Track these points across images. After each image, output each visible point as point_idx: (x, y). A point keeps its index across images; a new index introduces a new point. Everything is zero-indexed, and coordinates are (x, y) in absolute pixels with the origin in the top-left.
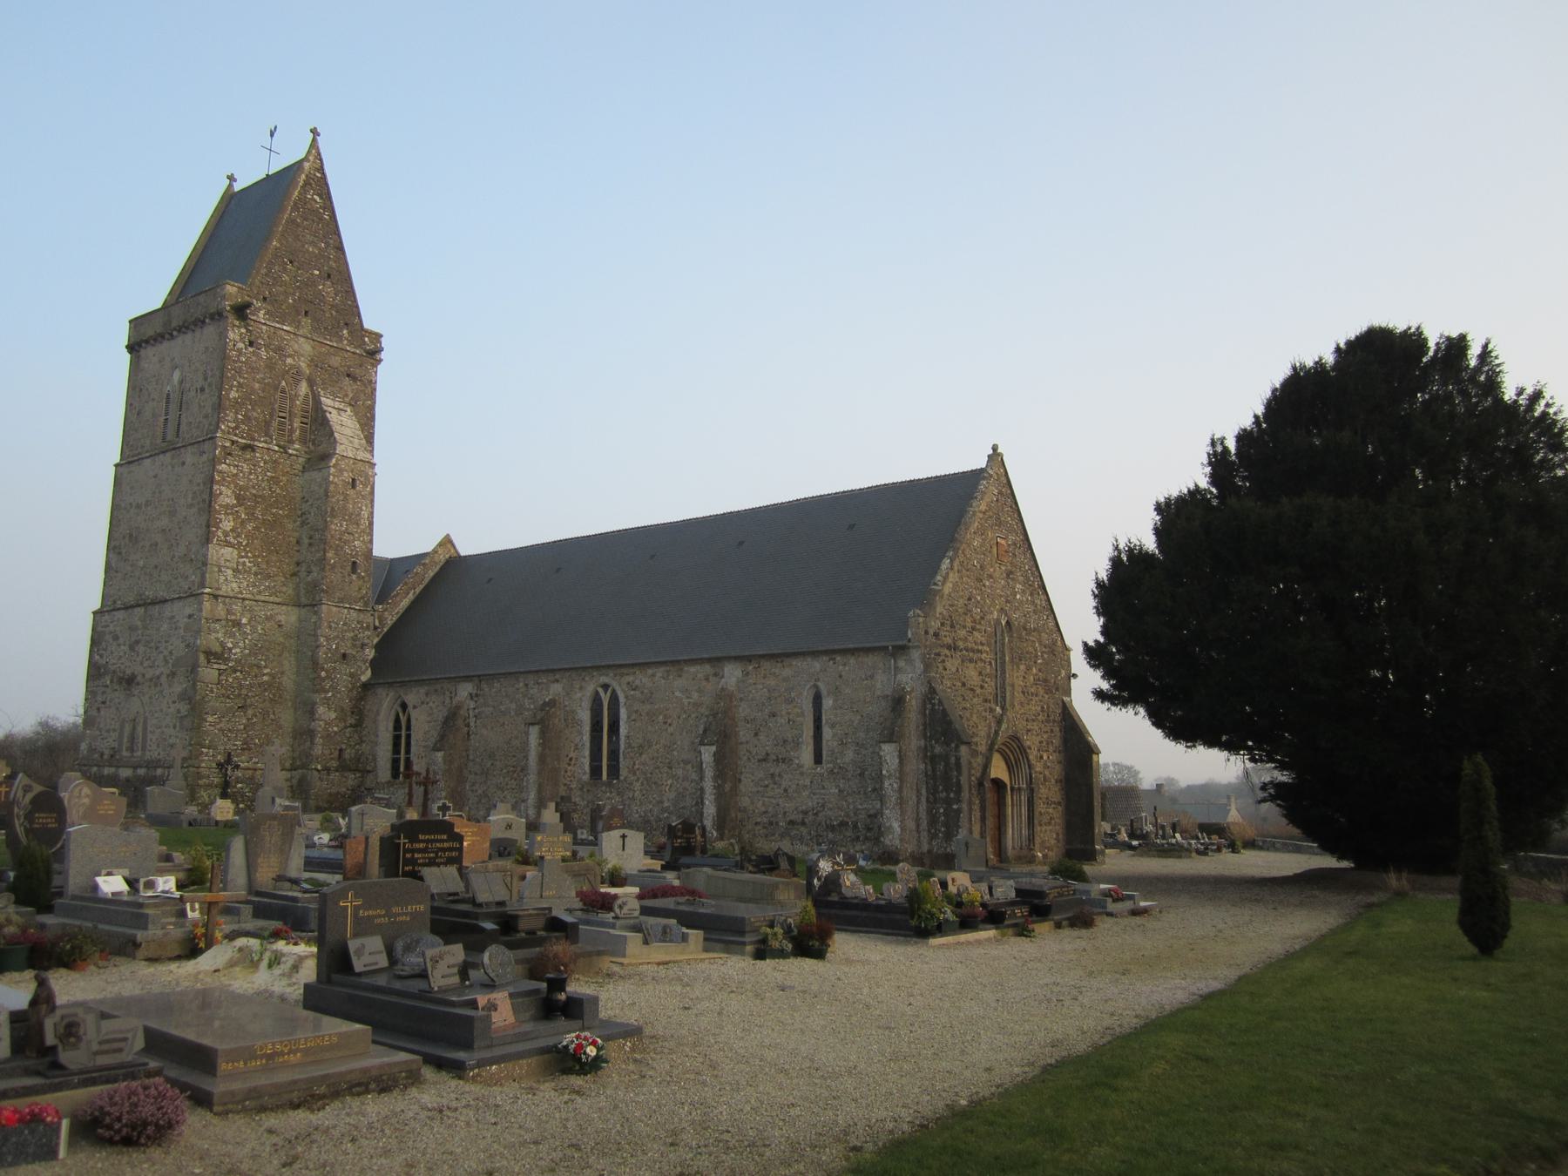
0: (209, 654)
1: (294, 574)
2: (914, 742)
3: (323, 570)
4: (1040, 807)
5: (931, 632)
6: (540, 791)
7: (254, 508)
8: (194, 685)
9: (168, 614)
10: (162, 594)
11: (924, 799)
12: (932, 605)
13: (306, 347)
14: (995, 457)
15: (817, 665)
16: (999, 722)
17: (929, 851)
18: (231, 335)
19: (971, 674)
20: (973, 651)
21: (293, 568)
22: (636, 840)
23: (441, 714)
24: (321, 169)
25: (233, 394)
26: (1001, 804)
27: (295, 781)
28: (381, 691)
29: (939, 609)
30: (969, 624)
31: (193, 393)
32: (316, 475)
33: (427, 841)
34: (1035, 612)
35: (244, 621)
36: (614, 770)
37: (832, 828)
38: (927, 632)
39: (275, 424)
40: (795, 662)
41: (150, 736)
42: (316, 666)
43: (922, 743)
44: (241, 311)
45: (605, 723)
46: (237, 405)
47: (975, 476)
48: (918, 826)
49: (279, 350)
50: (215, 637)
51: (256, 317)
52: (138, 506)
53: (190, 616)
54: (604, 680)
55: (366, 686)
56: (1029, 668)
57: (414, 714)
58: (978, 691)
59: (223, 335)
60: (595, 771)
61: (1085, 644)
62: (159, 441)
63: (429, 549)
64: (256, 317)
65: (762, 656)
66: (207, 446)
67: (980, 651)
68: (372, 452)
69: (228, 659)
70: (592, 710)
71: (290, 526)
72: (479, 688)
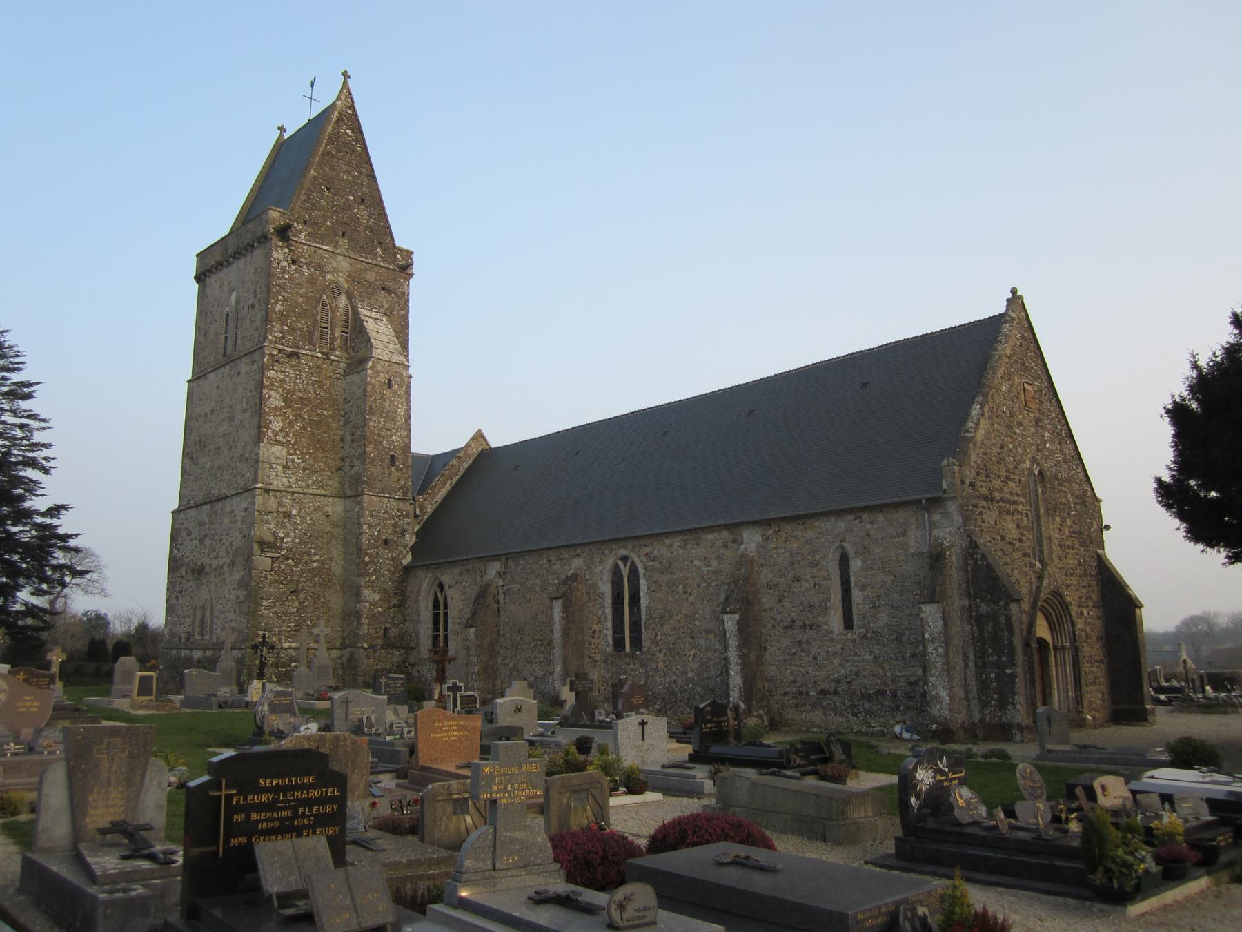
0: (262, 543)
1: (339, 469)
2: (957, 602)
3: (364, 463)
4: (1085, 667)
5: (967, 481)
6: (565, 665)
7: (301, 409)
8: (250, 572)
9: (228, 509)
10: (225, 492)
11: (971, 664)
12: (966, 453)
13: (344, 264)
14: (1015, 300)
15: (841, 525)
16: (1040, 577)
17: (982, 721)
18: (275, 254)
19: (1009, 526)
20: (1009, 502)
21: (338, 463)
22: (658, 726)
23: (473, 592)
24: (352, 107)
25: (279, 308)
26: (1044, 664)
27: (345, 659)
28: (420, 573)
29: (973, 458)
30: (1004, 474)
31: (246, 310)
32: (355, 378)
33: (277, 789)
34: (1065, 461)
35: (294, 512)
36: (637, 642)
37: (868, 697)
38: (963, 483)
39: (318, 334)
40: (820, 524)
41: (216, 621)
42: (359, 548)
43: (966, 602)
44: (283, 233)
45: (625, 595)
46: (282, 317)
47: (992, 325)
48: (967, 693)
49: (320, 267)
50: (267, 528)
51: (307, 245)
52: (206, 416)
53: (246, 510)
54: (623, 552)
55: (407, 569)
56: (1063, 520)
57: (450, 593)
58: (1018, 545)
59: (268, 256)
60: (619, 643)
61: (1159, 480)
62: (221, 357)
63: (462, 445)
64: (307, 245)
65: (783, 519)
66: (257, 356)
67: (1015, 502)
68: (407, 357)
69: (280, 548)
70: (612, 582)
71: (334, 425)
72: (506, 565)
